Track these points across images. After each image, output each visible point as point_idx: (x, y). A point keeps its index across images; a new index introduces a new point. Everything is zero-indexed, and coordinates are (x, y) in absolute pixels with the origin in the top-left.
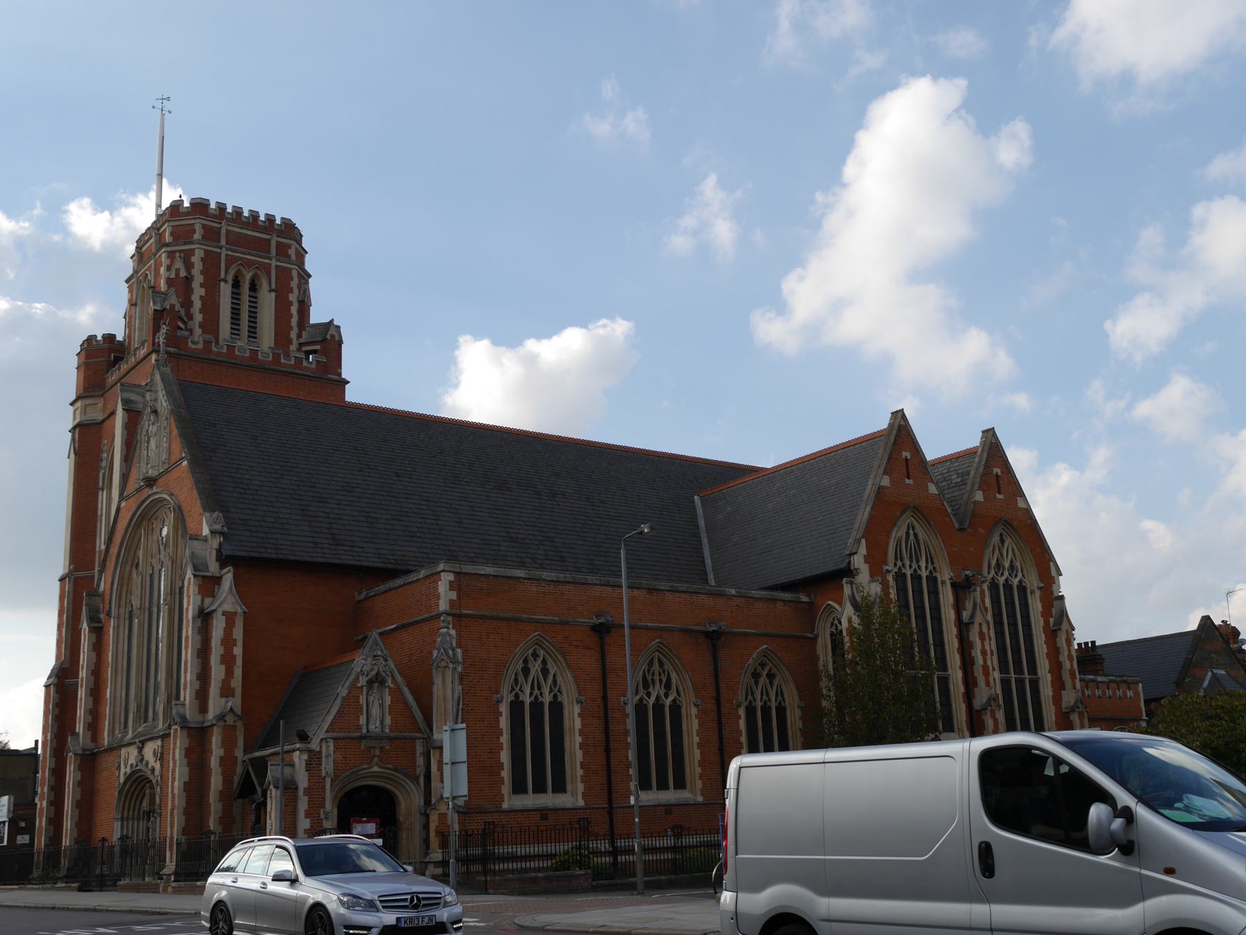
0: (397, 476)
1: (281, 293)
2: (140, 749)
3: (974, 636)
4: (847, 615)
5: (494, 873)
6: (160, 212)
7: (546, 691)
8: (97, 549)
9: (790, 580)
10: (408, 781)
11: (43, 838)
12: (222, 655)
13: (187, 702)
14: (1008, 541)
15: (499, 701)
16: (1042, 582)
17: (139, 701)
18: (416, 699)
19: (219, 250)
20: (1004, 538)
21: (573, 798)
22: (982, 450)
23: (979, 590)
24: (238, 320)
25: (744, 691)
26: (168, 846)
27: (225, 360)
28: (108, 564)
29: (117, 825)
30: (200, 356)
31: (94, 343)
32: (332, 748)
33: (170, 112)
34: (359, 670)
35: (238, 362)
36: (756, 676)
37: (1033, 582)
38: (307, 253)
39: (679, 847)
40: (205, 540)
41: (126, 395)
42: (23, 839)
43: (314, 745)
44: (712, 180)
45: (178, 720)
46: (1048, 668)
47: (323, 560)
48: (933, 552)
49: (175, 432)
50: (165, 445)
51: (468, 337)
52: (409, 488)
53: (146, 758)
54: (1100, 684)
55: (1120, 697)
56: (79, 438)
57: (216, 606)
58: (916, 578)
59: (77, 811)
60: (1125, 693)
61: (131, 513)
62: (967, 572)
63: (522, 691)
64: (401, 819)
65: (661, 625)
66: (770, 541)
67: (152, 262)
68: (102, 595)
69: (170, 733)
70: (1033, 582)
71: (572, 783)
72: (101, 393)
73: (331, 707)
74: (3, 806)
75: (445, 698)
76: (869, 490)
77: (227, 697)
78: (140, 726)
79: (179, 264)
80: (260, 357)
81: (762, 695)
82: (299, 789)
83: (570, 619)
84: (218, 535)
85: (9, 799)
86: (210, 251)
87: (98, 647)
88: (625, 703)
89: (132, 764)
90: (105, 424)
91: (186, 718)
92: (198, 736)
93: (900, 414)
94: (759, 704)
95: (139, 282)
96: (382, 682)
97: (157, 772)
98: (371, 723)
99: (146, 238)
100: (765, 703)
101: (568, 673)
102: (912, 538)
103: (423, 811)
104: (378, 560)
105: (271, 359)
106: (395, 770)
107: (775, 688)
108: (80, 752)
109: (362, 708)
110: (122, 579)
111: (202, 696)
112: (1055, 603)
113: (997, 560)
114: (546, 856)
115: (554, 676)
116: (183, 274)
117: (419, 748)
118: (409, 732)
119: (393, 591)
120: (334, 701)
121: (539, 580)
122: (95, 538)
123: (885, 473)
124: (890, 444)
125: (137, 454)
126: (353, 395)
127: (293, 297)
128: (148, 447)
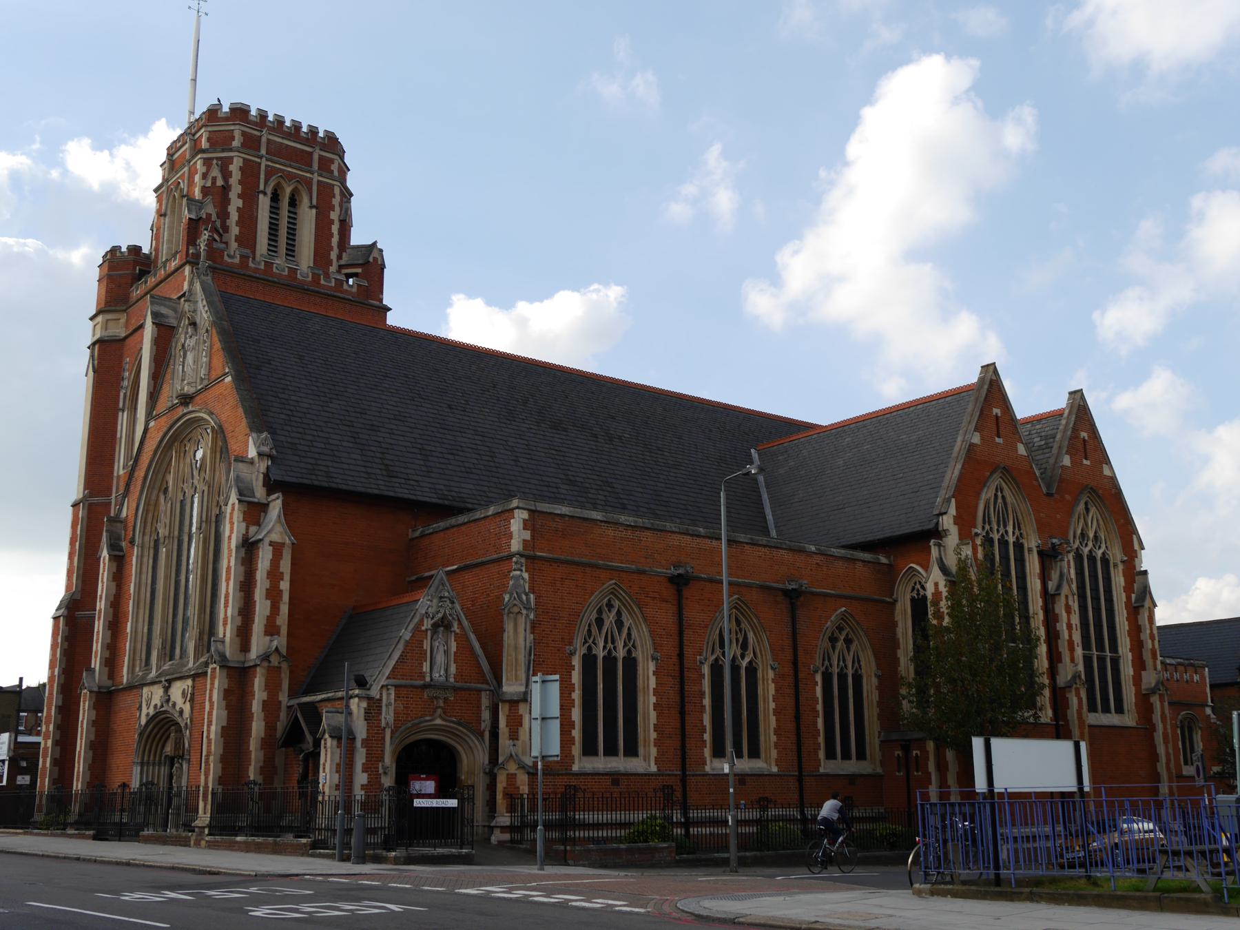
0: (451, 408)
1: (323, 210)
2: (167, 689)
3: (1060, 609)
4: (934, 582)
5: (574, 841)
6: (192, 119)
7: (620, 644)
8: (115, 474)
9: (868, 539)
10: (472, 736)
11: (47, 780)
12: (267, 589)
13: (228, 639)
14: (1093, 510)
15: (572, 654)
16: (1126, 556)
17: (202, 628)
18: (483, 646)
19: (259, 160)
20: (1089, 506)
21: (645, 763)
22: (1070, 413)
23: (1066, 560)
24: (277, 236)
25: (821, 656)
26: (201, 795)
27: (262, 276)
28: (132, 488)
29: (137, 770)
30: (236, 270)
31: (118, 254)
32: (393, 696)
33: (206, 14)
34: (424, 612)
35: (276, 280)
36: (833, 640)
37: (1116, 555)
38: (349, 170)
39: (764, 820)
40: (252, 462)
41: (157, 308)
42: (23, 780)
43: (374, 692)
44: (716, 149)
45: (216, 657)
46: (1129, 647)
47: (376, 492)
48: (1020, 518)
49: (218, 345)
50: (204, 359)
51: (461, 296)
52: (463, 422)
53: (173, 699)
54: (1168, 666)
55: (1187, 681)
56: (99, 355)
57: (263, 535)
58: (1003, 543)
59: (91, 753)
60: (1192, 677)
61: (161, 434)
62: (1054, 541)
63: (595, 644)
64: (463, 778)
65: (740, 580)
66: (841, 498)
67: (186, 169)
68: (124, 522)
69: (206, 672)
70: (1116, 555)
71: (645, 746)
72: (124, 308)
73: (393, 650)
74: (2, 743)
75: (516, 648)
76: (959, 446)
77: (272, 635)
78: (165, 664)
79: (215, 172)
80: (299, 276)
81: (839, 661)
82: (357, 740)
83: (647, 569)
84: (265, 458)
85: (10, 736)
86: (250, 160)
87: (119, 577)
88: (702, 663)
89: (156, 705)
90: (127, 341)
91: (226, 657)
92: (239, 676)
93: (991, 368)
94: (835, 670)
95: (169, 191)
96: (448, 627)
97: (187, 714)
98: (435, 670)
99: (178, 145)
100: (842, 669)
101: (644, 626)
102: (1000, 500)
103: (487, 770)
104: (434, 496)
105: (310, 279)
106: (460, 724)
107: (852, 654)
108: (96, 689)
109: (426, 654)
110: (148, 505)
111: (244, 633)
112: (1137, 578)
113: (1082, 530)
114: (616, 824)
115: (629, 629)
116: (220, 182)
117: (485, 701)
118: (475, 683)
119: (455, 529)
120: (397, 644)
121: (616, 524)
122: (114, 463)
123: (976, 429)
124: (982, 399)
125: (169, 370)
126: (392, 320)
127: (334, 216)
128: (184, 362)
